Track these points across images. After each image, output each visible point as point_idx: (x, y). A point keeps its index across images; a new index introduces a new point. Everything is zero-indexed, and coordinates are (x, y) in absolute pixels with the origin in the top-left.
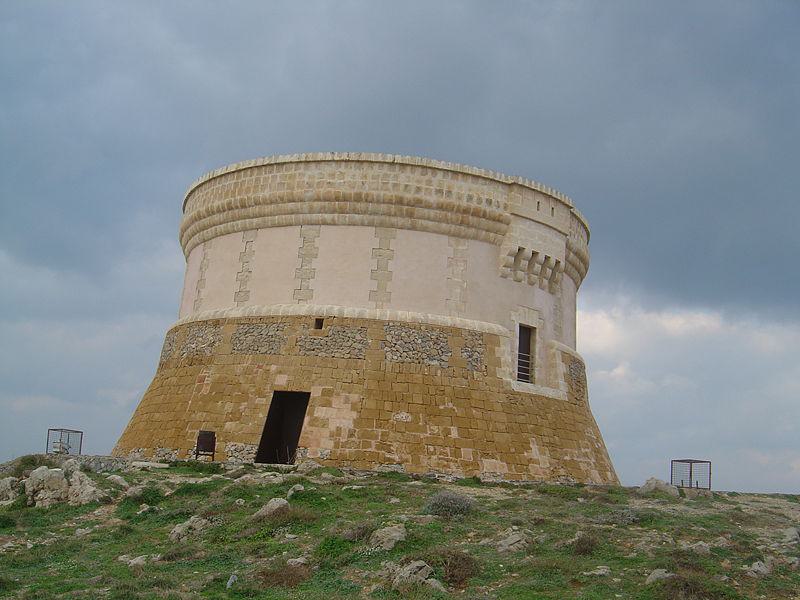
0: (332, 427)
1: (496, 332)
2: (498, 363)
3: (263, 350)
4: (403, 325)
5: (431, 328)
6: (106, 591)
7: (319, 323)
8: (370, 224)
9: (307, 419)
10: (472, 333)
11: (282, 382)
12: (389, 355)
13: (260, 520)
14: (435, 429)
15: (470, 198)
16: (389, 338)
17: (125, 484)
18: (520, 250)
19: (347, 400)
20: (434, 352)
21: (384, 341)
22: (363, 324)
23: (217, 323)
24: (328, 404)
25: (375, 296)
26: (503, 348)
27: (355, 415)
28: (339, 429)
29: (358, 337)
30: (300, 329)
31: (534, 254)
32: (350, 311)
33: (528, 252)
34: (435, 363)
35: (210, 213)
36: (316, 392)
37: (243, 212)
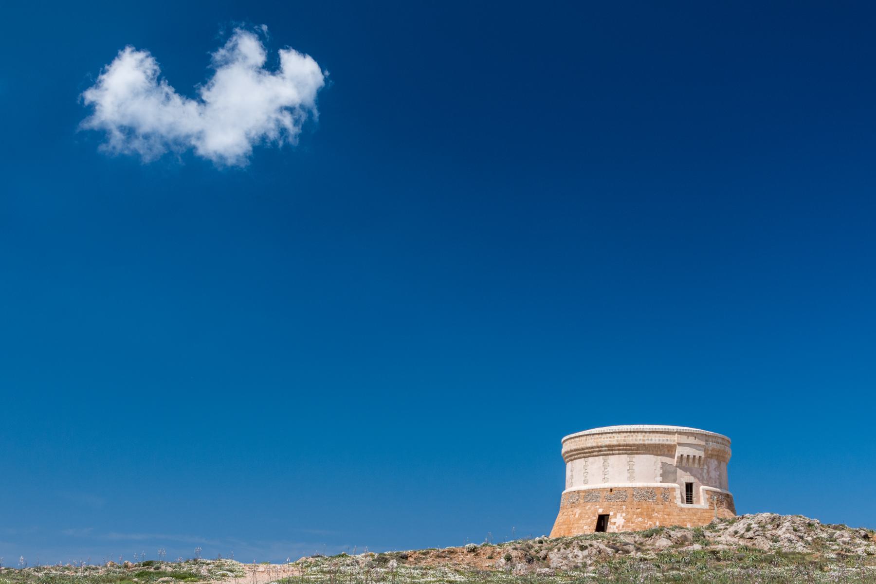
0: (617, 525)
1: (674, 487)
2: (675, 498)
3: (594, 501)
4: (639, 488)
5: (649, 488)
6: (577, 582)
7: (611, 490)
8: (626, 454)
9: (609, 523)
10: (664, 488)
11: (601, 511)
12: (635, 499)
13: (687, 553)
14: (651, 523)
15: (659, 440)
16: (634, 493)
17: (87, 573)
18: (682, 455)
19: (621, 516)
20: (650, 497)
21: (633, 495)
22: (626, 489)
23: (578, 492)
24: (616, 518)
25: (631, 478)
26: (677, 492)
27: (624, 520)
28: (619, 525)
29: (624, 494)
30: (605, 493)
31: (694, 456)
32: (621, 485)
33: (691, 457)
34: (651, 500)
35: (571, 451)
36: (611, 514)
37: (583, 451)
